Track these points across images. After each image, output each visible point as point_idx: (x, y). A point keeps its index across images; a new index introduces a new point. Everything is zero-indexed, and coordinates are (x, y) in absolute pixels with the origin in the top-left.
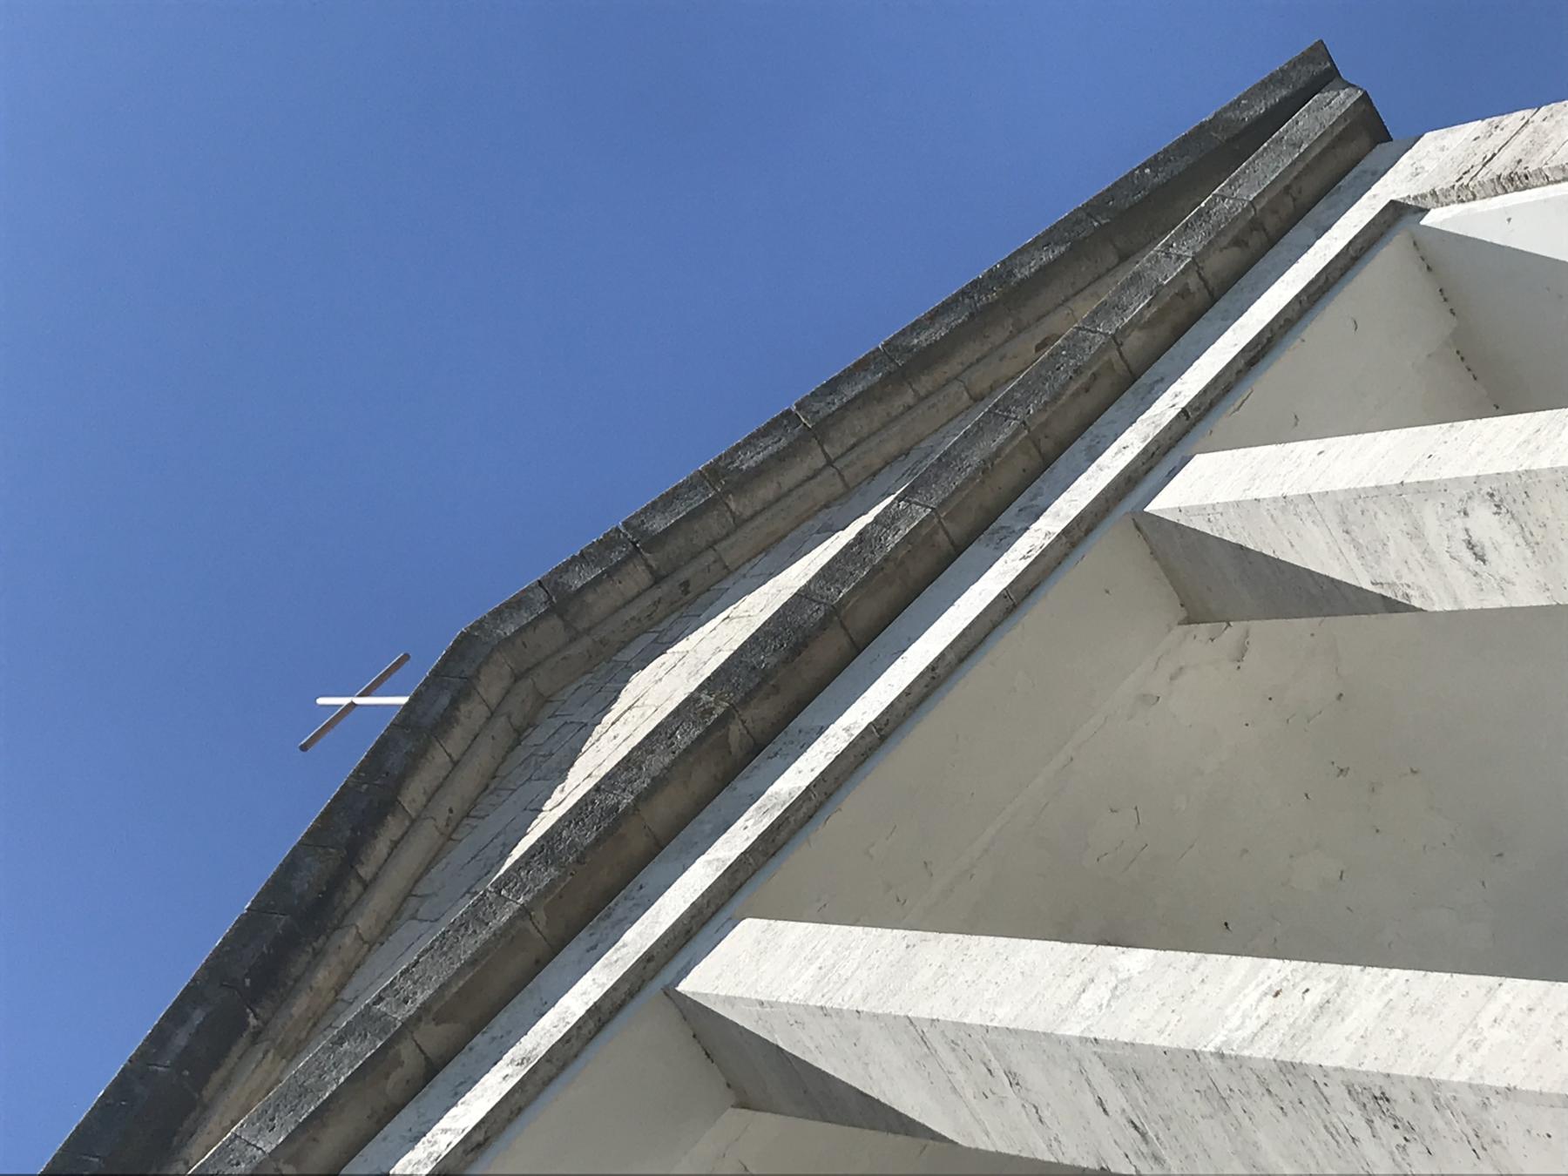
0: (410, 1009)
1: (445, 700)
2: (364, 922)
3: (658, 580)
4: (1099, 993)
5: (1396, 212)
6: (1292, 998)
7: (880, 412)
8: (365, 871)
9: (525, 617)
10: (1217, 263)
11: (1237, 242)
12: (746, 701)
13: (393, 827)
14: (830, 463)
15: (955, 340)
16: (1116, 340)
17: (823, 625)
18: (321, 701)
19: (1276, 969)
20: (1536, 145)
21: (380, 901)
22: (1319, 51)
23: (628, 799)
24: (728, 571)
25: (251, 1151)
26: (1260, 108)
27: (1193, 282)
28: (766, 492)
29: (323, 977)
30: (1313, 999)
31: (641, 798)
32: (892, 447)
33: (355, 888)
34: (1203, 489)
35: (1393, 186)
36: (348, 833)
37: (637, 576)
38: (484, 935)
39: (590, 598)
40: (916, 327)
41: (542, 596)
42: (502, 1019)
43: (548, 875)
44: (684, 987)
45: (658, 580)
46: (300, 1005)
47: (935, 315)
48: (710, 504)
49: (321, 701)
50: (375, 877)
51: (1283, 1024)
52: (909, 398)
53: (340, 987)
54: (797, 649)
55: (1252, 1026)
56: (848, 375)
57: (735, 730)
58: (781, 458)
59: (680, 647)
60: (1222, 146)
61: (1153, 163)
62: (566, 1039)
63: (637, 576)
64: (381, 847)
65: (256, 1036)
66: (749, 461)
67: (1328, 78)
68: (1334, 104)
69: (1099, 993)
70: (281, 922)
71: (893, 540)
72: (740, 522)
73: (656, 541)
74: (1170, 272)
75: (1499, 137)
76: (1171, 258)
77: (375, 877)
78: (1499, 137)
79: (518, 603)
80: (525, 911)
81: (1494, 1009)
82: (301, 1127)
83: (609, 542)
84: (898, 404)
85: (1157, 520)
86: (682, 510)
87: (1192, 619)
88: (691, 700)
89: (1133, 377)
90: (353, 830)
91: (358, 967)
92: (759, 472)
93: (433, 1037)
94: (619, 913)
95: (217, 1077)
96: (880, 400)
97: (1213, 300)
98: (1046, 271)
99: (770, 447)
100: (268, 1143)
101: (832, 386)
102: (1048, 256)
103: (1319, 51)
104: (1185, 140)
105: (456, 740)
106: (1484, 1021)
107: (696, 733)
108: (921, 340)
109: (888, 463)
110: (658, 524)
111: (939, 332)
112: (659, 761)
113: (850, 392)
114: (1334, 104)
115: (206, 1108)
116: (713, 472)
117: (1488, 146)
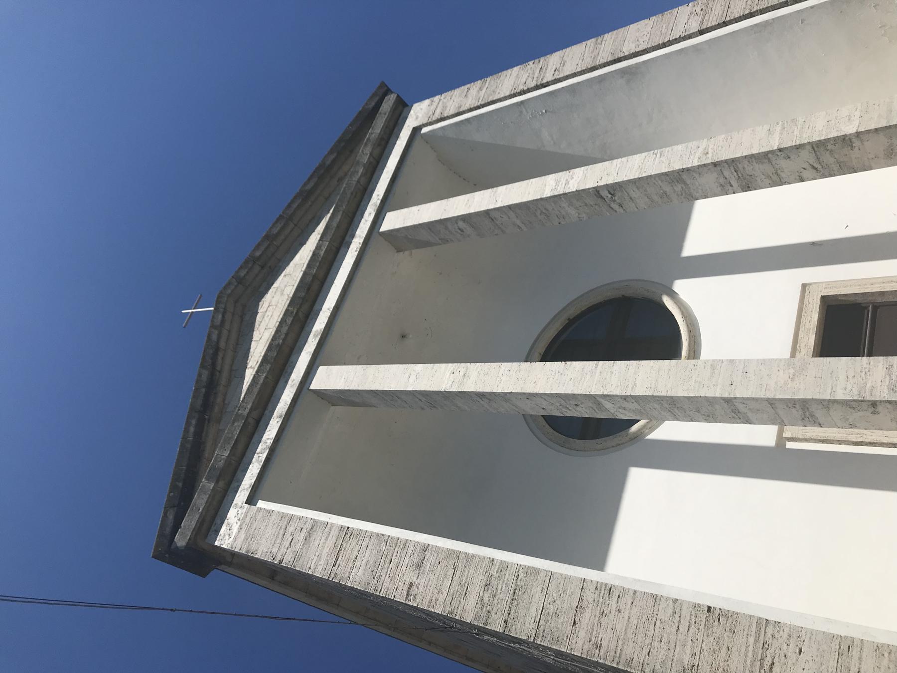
0: (247, 410)
1: (220, 316)
2: (223, 381)
3: (262, 267)
4: (413, 378)
5: (416, 130)
6: (457, 373)
8: (218, 368)
9: (232, 287)
10: (377, 152)
11: (379, 145)
12: (300, 307)
13: (221, 355)
14: (296, 225)
15: (316, 185)
16: (358, 182)
17: (312, 281)
19: (451, 366)
20: (445, 107)
21: (225, 374)
22: (383, 85)
23: (281, 341)
24: (279, 260)
26: (373, 104)
27: (372, 160)
28: (282, 237)
29: (219, 400)
30: (462, 373)
31: (284, 340)
33: (218, 373)
34: (394, 221)
35: (411, 123)
37: (257, 268)
38: (258, 386)
40: (305, 184)
42: (270, 406)
43: (268, 367)
44: (312, 387)
45: (262, 267)
46: (216, 409)
47: (309, 179)
48: (269, 245)
51: (457, 381)
52: (310, 203)
53: (224, 400)
54: (309, 289)
55: (450, 383)
56: (292, 202)
57: (300, 314)
58: (283, 229)
59: (275, 285)
60: (368, 116)
61: (351, 125)
62: (289, 408)
63: (257, 268)
65: (209, 420)
66: (275, 231)
67: (388, 92)
68: (390, 100)
69: (413, 378)
71: (322, 253)
73: (259, 258)
74: (365, 159)
75: (435, 104)
76: (364, 153)
78: (435, 104)
79: (229, 283)
80: (266, 377)
81: (502, 371)
82: (232, 448)
83: (246, 262)
85: (383, 233)
86: (262, 248)
87: (398, 252)
88: (287, 310)
89: (365, 189)
92: (279, 233)
93: (255, 414)
94: (289, 371)
95: (204, 434)
97: (378, 162)
98: (334, 161)
99: (279, 226)
100: (226, 453)
101: (289, 206)
102: (333, 157)
103: (383, 85)
104: (357, 117)
105: (227, 326)
106: (500, 375)
107: (291, 319)
108: (308, 187)
109: (310, 221)
110: (258, 254)
111: (311, 184)
112: (285, 329)
113: (295, 206)
114: (390, 100)
116: (267, 237)
117: (433, 107)
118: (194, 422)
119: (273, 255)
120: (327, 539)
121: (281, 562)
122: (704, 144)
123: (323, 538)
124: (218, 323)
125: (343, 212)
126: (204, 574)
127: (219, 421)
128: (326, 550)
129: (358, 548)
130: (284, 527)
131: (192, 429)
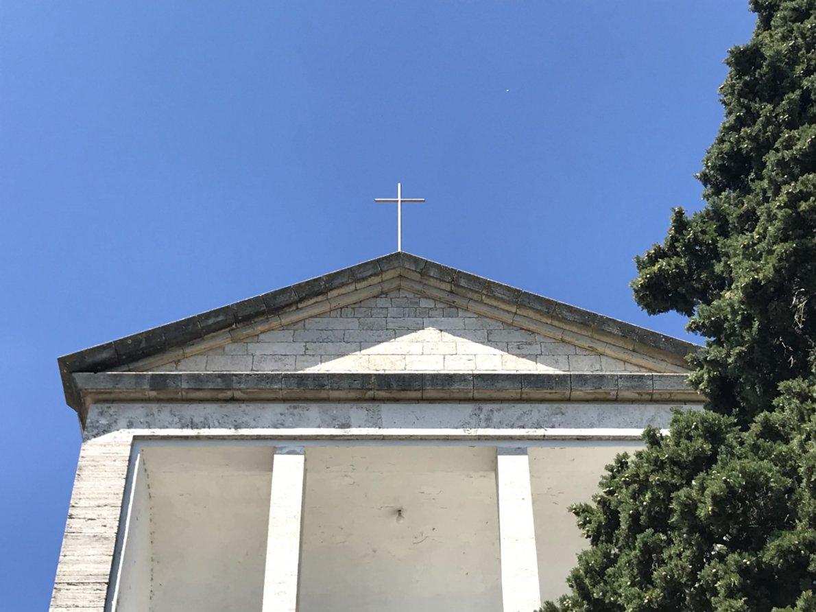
2: (285, 320)
3: (451, 292)
7: (538, 317)
8: (300, 306)
13: (320, 298)
14: (516, 313)
18: (399, 185)
25: (179, 383)
28: (495, 303)
29: (260, 328)
32: (532, 327)
36: (304, 295)
39: (432, 279)
41: (422, 267)
45: (451, 292)
46: (249, 331)
49: (399, 185)
50: (301, 309)
52: (549, 321)
64: (312, 301)
70: (264, 308)
72: (481, 302)
73: (458, 286)
77: (301, 309)
84: (544, 320)
90: (306, 295)
91: (273, 330)
96: (541, 315)
115: (203, 339)
118: (221, 318)
119: (471, 299)
120: (95, 562)
121: (71, 517)
122: (777, 542)
123: (95, 558)
124: (359, 276)
125: (785, 71)
126: (68, 404)
127: (234, 341)
128: (81, 567)
129: (86, 604)
130: (106, 502)
131: (211, 321)
